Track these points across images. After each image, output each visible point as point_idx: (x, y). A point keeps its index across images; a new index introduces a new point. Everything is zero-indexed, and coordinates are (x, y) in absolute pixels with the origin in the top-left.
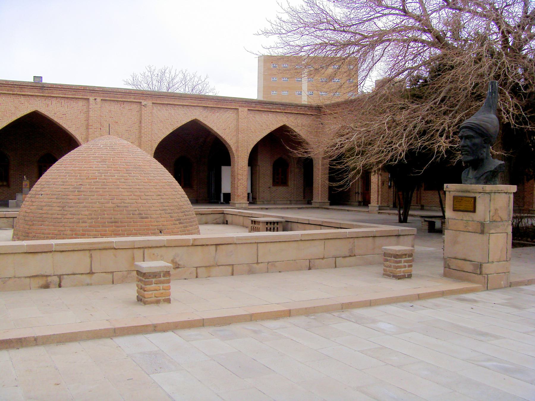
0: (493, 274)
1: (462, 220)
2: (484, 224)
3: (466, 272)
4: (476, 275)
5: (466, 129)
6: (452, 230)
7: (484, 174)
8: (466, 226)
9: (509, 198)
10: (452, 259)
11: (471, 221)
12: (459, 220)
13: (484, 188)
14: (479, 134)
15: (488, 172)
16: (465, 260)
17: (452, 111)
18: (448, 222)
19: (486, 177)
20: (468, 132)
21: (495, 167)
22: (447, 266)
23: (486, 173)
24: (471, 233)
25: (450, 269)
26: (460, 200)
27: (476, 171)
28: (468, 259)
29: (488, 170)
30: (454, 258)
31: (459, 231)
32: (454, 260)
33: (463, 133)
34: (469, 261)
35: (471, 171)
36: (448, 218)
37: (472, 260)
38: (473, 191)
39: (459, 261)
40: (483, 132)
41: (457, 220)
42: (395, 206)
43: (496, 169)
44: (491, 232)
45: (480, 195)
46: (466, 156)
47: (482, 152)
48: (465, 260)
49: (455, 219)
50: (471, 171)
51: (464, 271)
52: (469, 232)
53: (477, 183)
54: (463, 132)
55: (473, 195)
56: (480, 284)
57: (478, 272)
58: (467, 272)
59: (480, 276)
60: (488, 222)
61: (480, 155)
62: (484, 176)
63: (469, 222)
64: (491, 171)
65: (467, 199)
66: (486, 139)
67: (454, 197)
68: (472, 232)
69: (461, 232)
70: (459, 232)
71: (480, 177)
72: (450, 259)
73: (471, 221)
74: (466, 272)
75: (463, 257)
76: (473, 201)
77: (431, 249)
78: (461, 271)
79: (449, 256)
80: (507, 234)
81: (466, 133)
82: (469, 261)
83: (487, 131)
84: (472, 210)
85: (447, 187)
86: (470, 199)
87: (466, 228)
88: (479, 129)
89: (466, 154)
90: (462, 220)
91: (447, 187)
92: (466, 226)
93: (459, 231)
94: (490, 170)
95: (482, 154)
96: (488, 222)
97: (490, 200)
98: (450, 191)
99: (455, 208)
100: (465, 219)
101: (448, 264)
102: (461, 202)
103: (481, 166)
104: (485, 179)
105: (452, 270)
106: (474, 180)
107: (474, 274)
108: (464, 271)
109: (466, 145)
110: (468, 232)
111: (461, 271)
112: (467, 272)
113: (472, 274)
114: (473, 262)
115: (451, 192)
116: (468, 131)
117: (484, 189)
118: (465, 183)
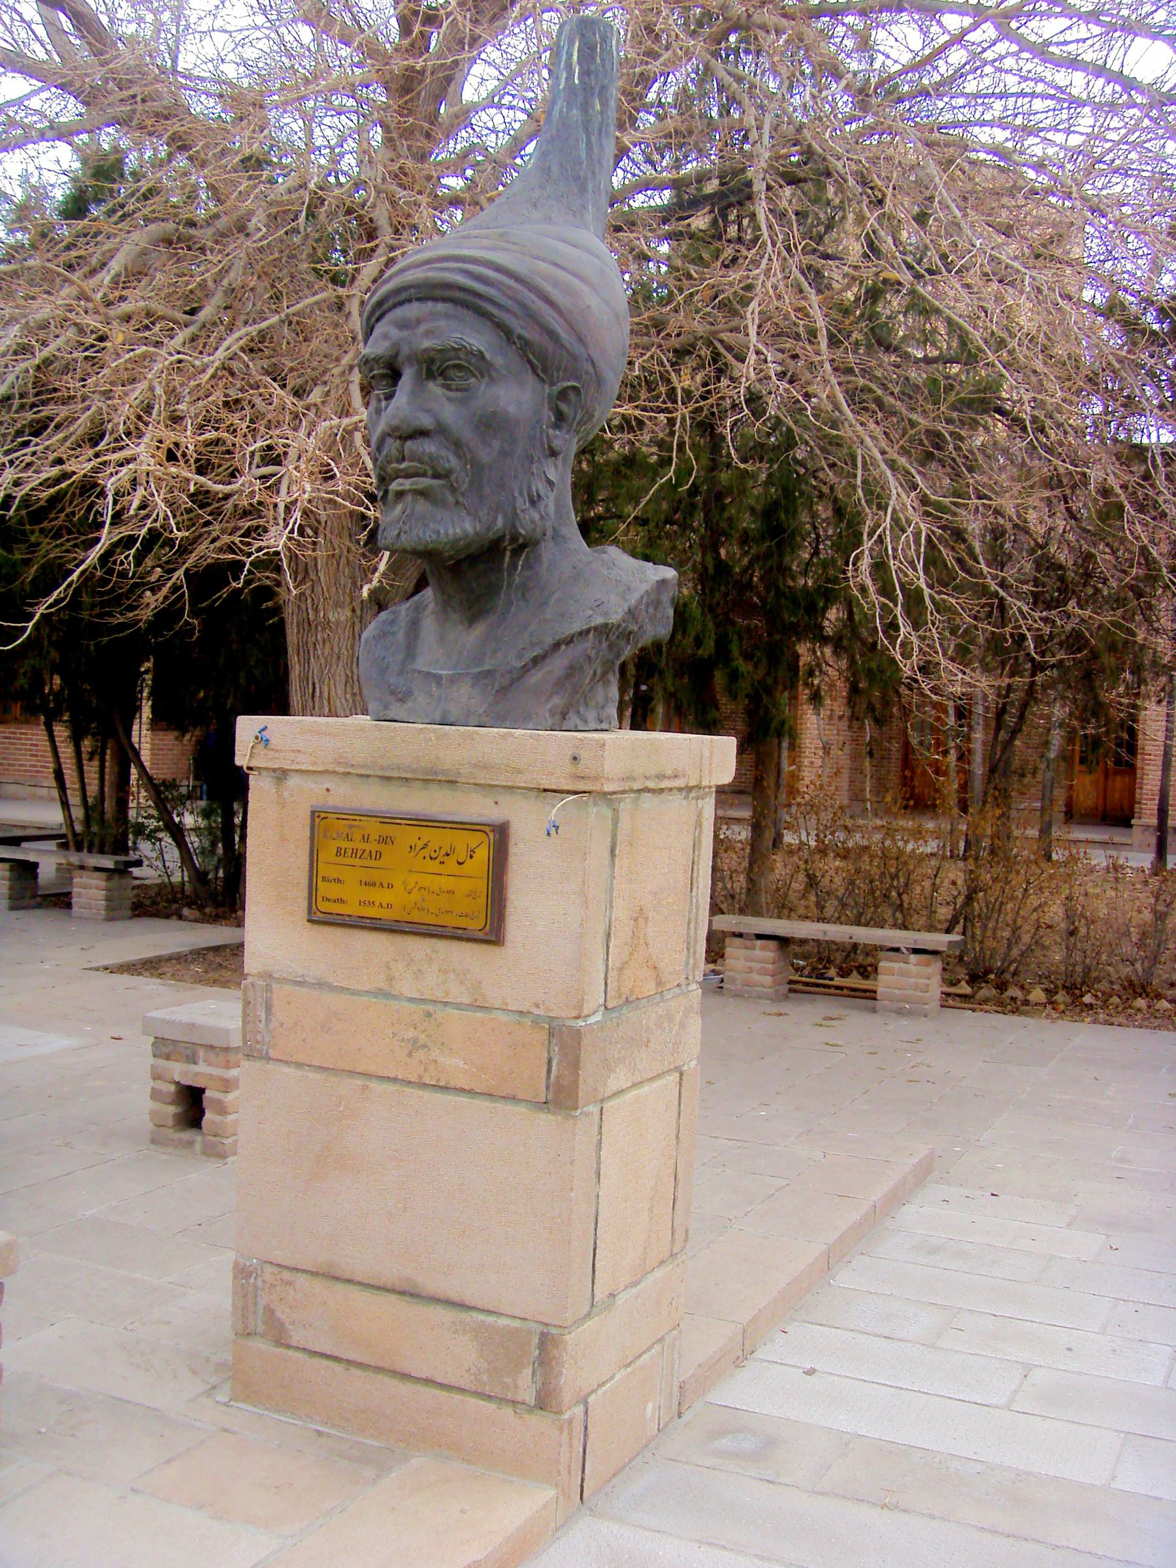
0: (612, 1378)
1: (380, 993)
2: (577, 1034)
3: (418, 1380)
4: (508, 1411)
5: (429, 306)
6: (299, 1065)
7: (556, 646)
8: (415, 1045)
9: (700, 816)
10: (302, 1280)
11: (459, 1006)
12: (358, 993)
13: (584, 755)
14: (524, 347)
15: (584, 633)
16: (410, 1293)
17: (192, 323)
18: (269, 1009)
19: (572, 670)
20: (442, 323)
21: (633, 600)
22: (261, 1328)
23: (569, 641)
24: (464, 1100)
25: (289, 1346)
26: (372, 847)
27: (479, 629)
28: (433, 1284)
29: (576, 627)
30: (315, 1274)
31: (352, 1073)
32: (318, 1287)
33: (395, 333)
34: (449, 1303)
35: (429, 626)
36: (268, 976)
37: (468, 1299)
38: (483, 778)
39: (361, 1299)
40: (552, 334)
41: (343, 990)
42: (84, 162)
43: (631, 613)
44: (613, 1084)
45: (555, 810)
46: (422, 506)
47: (539, 486)
48: (410, 1293)
49: (321, 985)
50: (429, 626)
51: (406, 1377)
52: (446, 1089)
53: (498, 719)
54: (404, 325)
55: (479, 808)
56: (155, 1019)
57: (526, 1388)
58: (428, 1382)
59: (539, 1422)
60: (598, 1017)
61: (522, 503)
62: (557, 664)
63: (439, 1012)
64: (603, 631)
65: (436, 838)
66: (563, 395)
67: (316, 815)
68: (471, 1093)
69: (374, 1085)
70: (359, 1082)
71: (525, 669)
72: (286, 1275)
73: (459, 1006)
74: (418, 1380)
75: (392, 1271)
76: (482, 854)
77: (54, 1043)
78: (379, 1369)
79: (279, 1256)
80: (681, 1075)
81: (428, 334)
82: (449, 1303)
83: (581, 340)
84: (475, 924)
85: (262, 740)
86: (474, 839)
87: (420, 1055)
88: (531, 316)
89: (422, 493)
90: (380, 993)
91: (262, 740)
92: (415, 1045)
93: (352, 1073)
94: (599, 620)
95: (534, 501)
96: (598, 1017)
97: (613, 851)
98: (281, 775)
99: (324, 906)
100: (407, 987)
101: (270, 1312)
102: (379, 855)
103: (525, 589)
104: (559, 684)
105: (300, 1355)
106: (465, 695)
107: (491, 1406)
108: (406, 1377)
109: (426, 422)
110: (436, 1087)
111: (379, 1369)
112: (428, 1382)
113: (472, 1401)
114: (481, 1317)
115: (293, 781)
116: (447, 316)
117: (581, 768)
118: (396, 710)
